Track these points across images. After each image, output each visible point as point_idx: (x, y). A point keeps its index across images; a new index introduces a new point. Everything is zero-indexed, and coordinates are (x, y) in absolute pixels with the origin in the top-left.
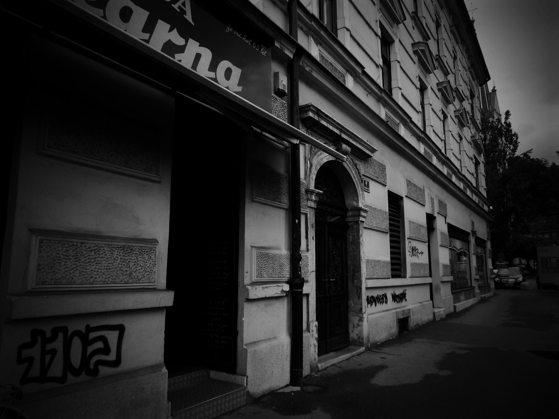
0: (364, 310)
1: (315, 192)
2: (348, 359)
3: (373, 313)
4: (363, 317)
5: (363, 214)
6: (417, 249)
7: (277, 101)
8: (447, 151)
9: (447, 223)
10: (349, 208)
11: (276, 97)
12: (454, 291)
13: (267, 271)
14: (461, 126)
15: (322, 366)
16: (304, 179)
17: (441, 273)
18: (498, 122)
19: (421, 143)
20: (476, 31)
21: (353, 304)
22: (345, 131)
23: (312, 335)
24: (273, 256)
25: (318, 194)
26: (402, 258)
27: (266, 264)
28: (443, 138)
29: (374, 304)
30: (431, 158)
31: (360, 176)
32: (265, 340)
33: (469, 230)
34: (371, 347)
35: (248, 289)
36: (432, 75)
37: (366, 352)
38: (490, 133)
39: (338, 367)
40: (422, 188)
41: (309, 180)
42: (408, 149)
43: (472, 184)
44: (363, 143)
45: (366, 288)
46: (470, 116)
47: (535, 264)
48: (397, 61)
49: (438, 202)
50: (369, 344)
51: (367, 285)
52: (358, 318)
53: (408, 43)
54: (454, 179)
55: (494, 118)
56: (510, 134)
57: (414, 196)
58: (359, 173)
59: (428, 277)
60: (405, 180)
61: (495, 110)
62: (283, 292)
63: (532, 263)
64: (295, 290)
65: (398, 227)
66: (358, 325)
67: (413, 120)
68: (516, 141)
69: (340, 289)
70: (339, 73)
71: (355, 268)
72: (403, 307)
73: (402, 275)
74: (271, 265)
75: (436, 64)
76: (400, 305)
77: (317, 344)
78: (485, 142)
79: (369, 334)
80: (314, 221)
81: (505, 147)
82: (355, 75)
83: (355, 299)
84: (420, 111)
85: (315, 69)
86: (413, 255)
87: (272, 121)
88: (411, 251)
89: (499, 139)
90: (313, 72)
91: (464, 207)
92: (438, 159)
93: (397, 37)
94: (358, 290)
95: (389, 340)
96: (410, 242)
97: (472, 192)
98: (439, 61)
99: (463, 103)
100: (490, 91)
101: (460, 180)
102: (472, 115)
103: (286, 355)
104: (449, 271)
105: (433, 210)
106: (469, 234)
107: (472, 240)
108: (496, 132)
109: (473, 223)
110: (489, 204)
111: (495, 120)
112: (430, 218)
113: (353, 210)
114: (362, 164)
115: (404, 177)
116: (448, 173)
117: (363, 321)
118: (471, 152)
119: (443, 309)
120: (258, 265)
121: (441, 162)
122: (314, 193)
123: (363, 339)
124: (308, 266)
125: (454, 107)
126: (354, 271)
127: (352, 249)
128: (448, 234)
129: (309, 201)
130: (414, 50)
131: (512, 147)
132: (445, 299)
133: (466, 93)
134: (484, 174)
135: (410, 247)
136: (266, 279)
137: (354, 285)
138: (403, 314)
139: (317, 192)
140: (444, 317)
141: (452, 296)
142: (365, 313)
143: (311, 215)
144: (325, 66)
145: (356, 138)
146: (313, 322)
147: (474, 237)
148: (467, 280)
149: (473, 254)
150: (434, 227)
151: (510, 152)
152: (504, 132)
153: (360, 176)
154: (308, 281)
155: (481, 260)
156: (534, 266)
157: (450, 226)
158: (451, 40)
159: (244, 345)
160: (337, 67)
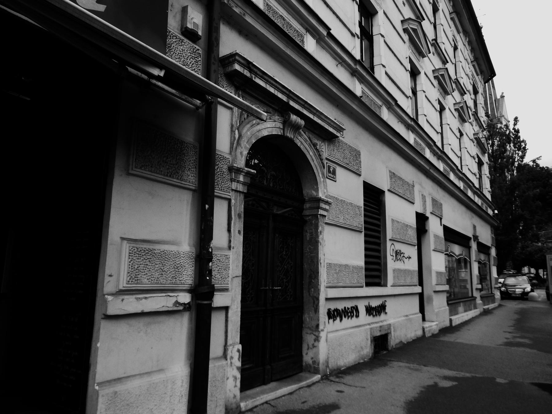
0: (321, 327)
1: (244, 170)
2: (291, 393)
3: (337, 331)
4: (319, 336)
5: (323, 205)
6: (403, 253)
7: (183, 43)
8: (445, 146)
9: (442, 225)
10: (307, 199)
11: (183, 38)
12: (450, 302)
13: (149, 274)
14: (461, 122)
15: (247, 405)
16: (228, 154)
17: (434, 281)
18: (506, 128)
19: (461, 181)
20: (482, 30)
21: (308, 319)
22: (295, 98)
23: (231, 363)
24: (162, 253)
25: (248, 173)
26: (382, 263)
27: (147, 265)
28: (409, 94)
29: (338, 319)
30: (423, 150)
31: (321, 160)
32: (141, 375)
33: (470, 234)
34: (330, 374)
35: (106, 301)
36: (426, 59)
37: (321, 382)
38: (498, 139)
39: (272, 406)
40: (411, 183)
41: (236, 155)
42: (403, 144)
43: (473, 184)
44: (323, 117)
45: (326, 298)
46: (473, 112)
47: (545, 273)
48: (380, 34)
49: (431, 201)
50: (328, 371)
51: (327, 295)
52: (314, 337)
53: (397, 19)
54: (452, 177)
55: (501, 123)
56: (519, 140)
57: (400, 191)
58: (320, 155)
59: (416, 286)
60: (388, 172)
61: (503, 116)
62: (178, 305)
63: (541, 272)
64: (199, 302)
65: (379, 226)
66: (314, 346)
67: (399, 102)
68: (524, 148)
69: (291, 299)
70: (295, 31)
71: (312, 273)
72: (382, 322)
73: (382, 283)
74: (157, 266)
75: (432, 49)
76: (377, 319)
77: (239, 376)
78: (493, 148)
79: (328, 358)
80: (242, 210)
81: (513, 153)
82: (318, 37)
83: (311, 313)
84: (410, 96)
85: (248, 12)
86: (397, 259)
87: (112, 36)
88: (394, 255)
89: (507, 145)
90: (246, 16)
91: (463, 209)
92: (433, 153)
93: (381, 8)
94: (315, 301)
95: (359, 363)
96: (393, 244)
97: (475, 193)
98: (436, 47)
99: (464, 96)
100: (498, 97)
101: (460, 179)
102: (474, 110)
103: (179, 394)
104: (444, 280)
105: (425, 209)
106: (470, 238)
107: (474, 246)
108: (504, 138)
109: (474, 227)
110: (493, 207)
111: (503, 126)
112: (421, 219)
113: (312, 201)
114: (325, 145)
115: (386, 167)
116: (444, 169)
117: (320, 341)
118: (474, 150)
119: (435, 323)
120: (131, 266)
121: (437, 157)
122: (242, 172)
123: (318, 365)
124: (229, 269)
125: (454, 100)
126: (310, 277)
127: (309, 249)
128: (443, 237)
129: (233, 183)
130: (404, 28)
131: (520, 153)
132: (438, 311)
133: (468, 87)
134: (488, 175)
135: (393, 250)
136: (146, 284)
137: (310, 294)
138: (380, 331)
139: (246, 171)
140: (436, 332)
141: (447, 308)
142: (322, 330)
143: (238, 202)
144: (272, 18)
145: (312, 109)
146: (234, 346)
147: (476, 242)
148: (468, 289)
149: (475, 261)
150: (427, 228)
151: (518, 158)
152: (512, 139)
153: (320, 159)
154: (228, 289)
155: (483, 266)
156: (544, 275)
157: (447, 230)
158: (450, 28)
159: (96, 384)
160: (291, 23)
